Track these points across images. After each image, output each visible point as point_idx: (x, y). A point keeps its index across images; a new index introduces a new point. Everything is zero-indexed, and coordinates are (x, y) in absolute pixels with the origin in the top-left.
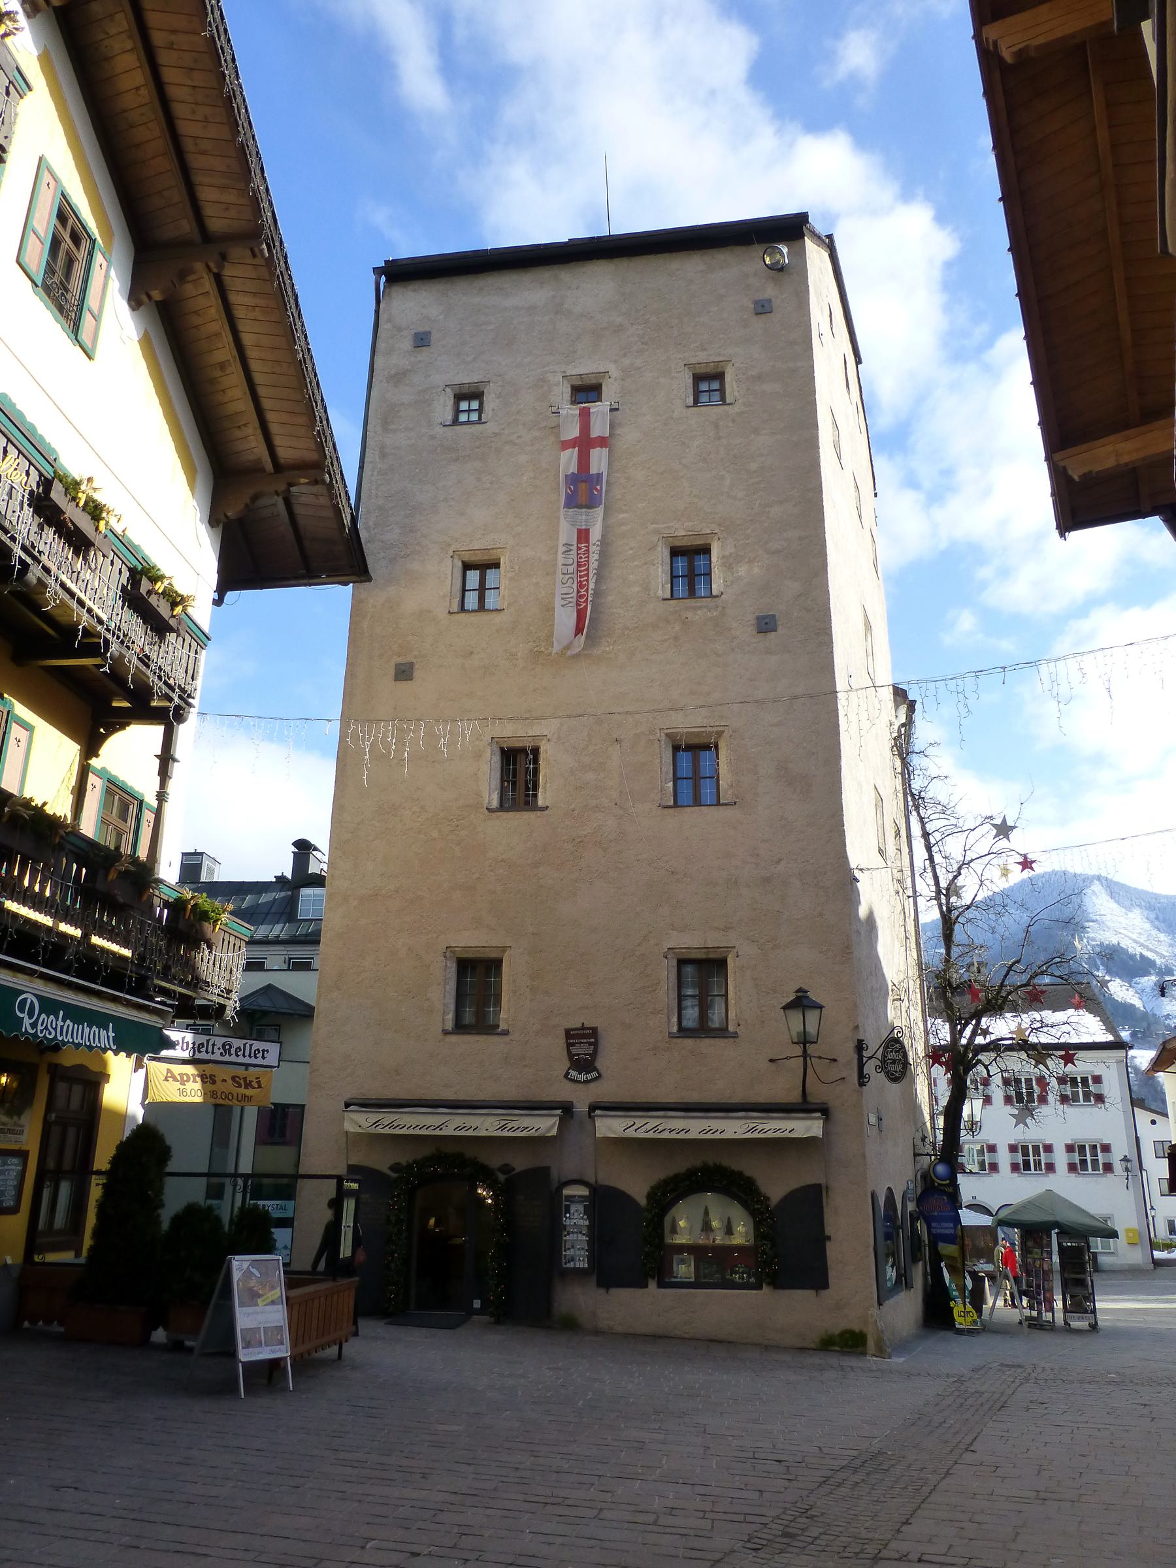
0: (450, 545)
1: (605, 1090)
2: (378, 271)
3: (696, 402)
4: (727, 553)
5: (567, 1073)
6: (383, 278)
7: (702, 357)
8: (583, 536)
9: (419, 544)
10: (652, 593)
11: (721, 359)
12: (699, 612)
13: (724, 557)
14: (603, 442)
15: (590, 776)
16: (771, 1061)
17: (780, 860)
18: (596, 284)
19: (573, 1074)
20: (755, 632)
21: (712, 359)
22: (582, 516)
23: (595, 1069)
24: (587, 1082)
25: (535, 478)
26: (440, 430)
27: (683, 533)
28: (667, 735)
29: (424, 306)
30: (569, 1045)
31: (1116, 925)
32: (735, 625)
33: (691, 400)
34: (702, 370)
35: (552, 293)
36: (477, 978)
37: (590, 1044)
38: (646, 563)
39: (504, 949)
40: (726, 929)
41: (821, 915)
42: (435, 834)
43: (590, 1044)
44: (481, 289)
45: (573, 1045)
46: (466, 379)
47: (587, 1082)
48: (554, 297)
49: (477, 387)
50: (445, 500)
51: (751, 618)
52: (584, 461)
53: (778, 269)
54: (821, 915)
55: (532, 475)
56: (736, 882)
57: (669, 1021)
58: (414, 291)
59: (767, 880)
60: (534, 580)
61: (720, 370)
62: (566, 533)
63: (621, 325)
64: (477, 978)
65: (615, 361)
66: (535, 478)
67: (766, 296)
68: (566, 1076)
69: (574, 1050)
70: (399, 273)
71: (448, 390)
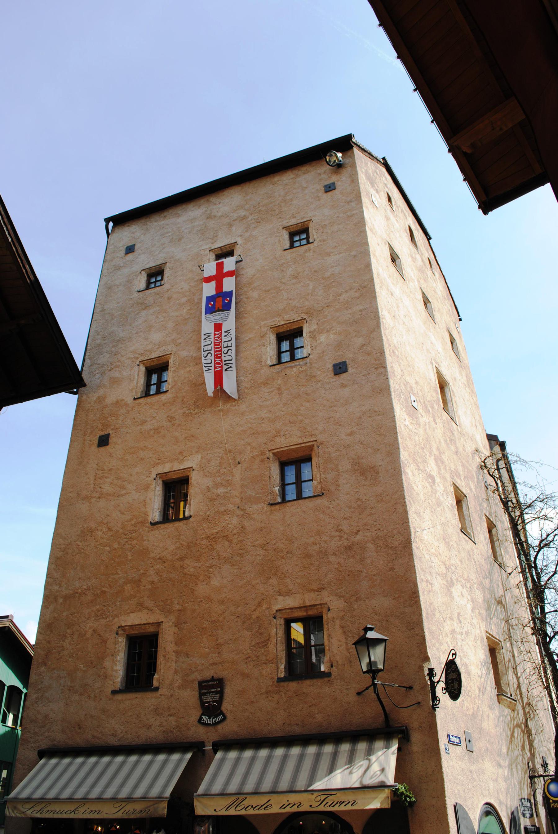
0: (138, 358)
1: (229, 728)
2: (107, 220)
3: (292, 246)
4: (312, 329)
5: (201, 718)
6: (111, 224)
7: (293, 222)
8: (218, 327)
9: (119, 361)
10: (263, 364)
11: (305, 220)
12: (294, 369)
13: (310, 332)
14: (230, 274)
15: (221, 490)
16: (359, 694)
17: (358, 531)
18: (232, 200)
19: (205, 718)
20: (332, 375)
21: (299, 221)
22: (217, 317)
23: (222, 713)
24: (216, 724)
25: (191, 309)
26: (136, 295)
27: (282, 323)
28: (273, 453)
29: (133, 233)
30: (201, 695)
31: (479, 596)
32: (319, 373)
33: (287, 245)
34: (294, 229)
35: (205, 209)
36: (143, 651)
37: (217, 692)
38: (259, 346)
39: (159, 624)
40: (320, 590)
41: (392, 569)
42: (116, 546)
43: (217, 692)
44: (165, 217)
45: (204, 694)
46: (152, 264)
47: (216, 724)
48: (206, 211)
49: (160, 268)
50: (137, 333)
51: (330, 366)
52: (219, 286)
53: (339, 166)
54: (392, 569)
55: (189, 308)
56: (325, 553)
57: (278, 668)
58: (129, 226)
59: (349, 548)
60: (188, 369)
61: (306, 226)
62: (207, 327)
63: (245, 216)
64: (143, 651)
65: (241, 236)
66: (191, 309)
67: (331, 182)
68: (200, 721)
69: (205, 699)
70: (120, 220)
71: (143, 272)
